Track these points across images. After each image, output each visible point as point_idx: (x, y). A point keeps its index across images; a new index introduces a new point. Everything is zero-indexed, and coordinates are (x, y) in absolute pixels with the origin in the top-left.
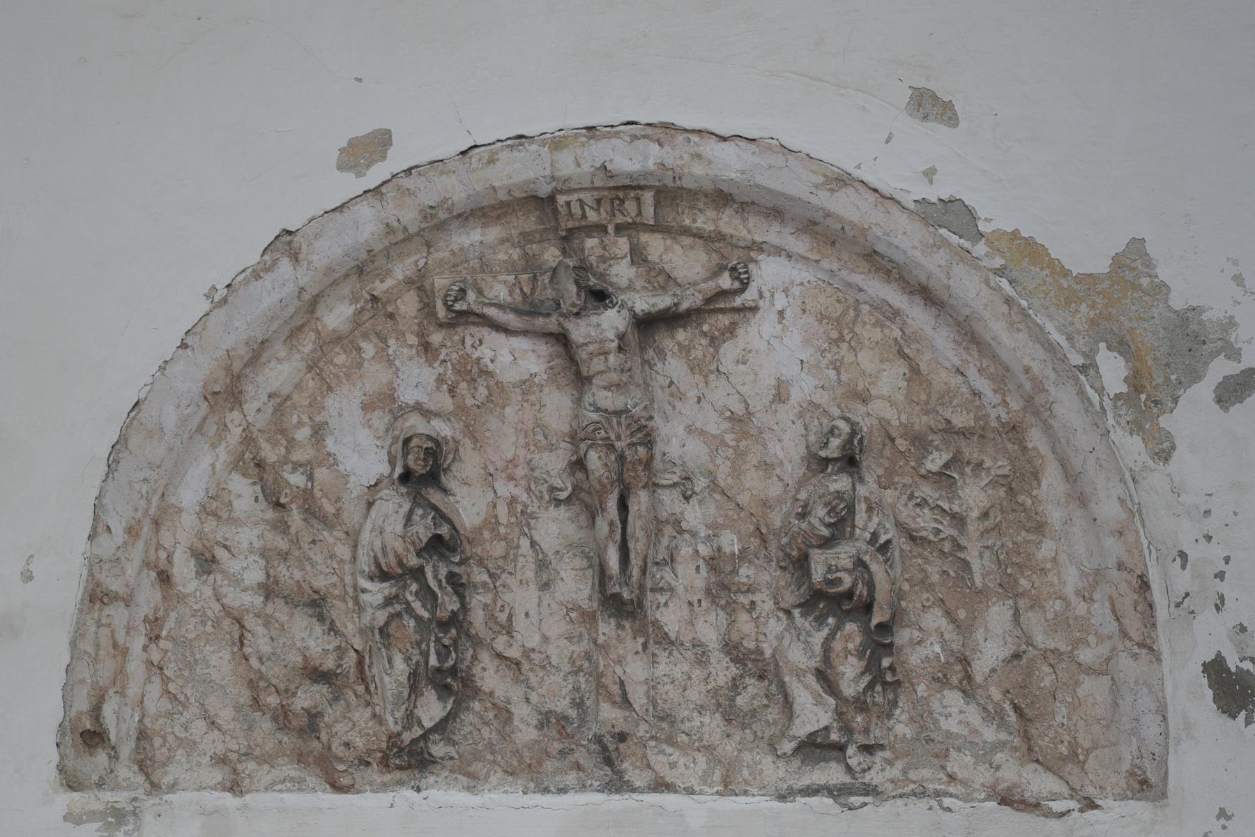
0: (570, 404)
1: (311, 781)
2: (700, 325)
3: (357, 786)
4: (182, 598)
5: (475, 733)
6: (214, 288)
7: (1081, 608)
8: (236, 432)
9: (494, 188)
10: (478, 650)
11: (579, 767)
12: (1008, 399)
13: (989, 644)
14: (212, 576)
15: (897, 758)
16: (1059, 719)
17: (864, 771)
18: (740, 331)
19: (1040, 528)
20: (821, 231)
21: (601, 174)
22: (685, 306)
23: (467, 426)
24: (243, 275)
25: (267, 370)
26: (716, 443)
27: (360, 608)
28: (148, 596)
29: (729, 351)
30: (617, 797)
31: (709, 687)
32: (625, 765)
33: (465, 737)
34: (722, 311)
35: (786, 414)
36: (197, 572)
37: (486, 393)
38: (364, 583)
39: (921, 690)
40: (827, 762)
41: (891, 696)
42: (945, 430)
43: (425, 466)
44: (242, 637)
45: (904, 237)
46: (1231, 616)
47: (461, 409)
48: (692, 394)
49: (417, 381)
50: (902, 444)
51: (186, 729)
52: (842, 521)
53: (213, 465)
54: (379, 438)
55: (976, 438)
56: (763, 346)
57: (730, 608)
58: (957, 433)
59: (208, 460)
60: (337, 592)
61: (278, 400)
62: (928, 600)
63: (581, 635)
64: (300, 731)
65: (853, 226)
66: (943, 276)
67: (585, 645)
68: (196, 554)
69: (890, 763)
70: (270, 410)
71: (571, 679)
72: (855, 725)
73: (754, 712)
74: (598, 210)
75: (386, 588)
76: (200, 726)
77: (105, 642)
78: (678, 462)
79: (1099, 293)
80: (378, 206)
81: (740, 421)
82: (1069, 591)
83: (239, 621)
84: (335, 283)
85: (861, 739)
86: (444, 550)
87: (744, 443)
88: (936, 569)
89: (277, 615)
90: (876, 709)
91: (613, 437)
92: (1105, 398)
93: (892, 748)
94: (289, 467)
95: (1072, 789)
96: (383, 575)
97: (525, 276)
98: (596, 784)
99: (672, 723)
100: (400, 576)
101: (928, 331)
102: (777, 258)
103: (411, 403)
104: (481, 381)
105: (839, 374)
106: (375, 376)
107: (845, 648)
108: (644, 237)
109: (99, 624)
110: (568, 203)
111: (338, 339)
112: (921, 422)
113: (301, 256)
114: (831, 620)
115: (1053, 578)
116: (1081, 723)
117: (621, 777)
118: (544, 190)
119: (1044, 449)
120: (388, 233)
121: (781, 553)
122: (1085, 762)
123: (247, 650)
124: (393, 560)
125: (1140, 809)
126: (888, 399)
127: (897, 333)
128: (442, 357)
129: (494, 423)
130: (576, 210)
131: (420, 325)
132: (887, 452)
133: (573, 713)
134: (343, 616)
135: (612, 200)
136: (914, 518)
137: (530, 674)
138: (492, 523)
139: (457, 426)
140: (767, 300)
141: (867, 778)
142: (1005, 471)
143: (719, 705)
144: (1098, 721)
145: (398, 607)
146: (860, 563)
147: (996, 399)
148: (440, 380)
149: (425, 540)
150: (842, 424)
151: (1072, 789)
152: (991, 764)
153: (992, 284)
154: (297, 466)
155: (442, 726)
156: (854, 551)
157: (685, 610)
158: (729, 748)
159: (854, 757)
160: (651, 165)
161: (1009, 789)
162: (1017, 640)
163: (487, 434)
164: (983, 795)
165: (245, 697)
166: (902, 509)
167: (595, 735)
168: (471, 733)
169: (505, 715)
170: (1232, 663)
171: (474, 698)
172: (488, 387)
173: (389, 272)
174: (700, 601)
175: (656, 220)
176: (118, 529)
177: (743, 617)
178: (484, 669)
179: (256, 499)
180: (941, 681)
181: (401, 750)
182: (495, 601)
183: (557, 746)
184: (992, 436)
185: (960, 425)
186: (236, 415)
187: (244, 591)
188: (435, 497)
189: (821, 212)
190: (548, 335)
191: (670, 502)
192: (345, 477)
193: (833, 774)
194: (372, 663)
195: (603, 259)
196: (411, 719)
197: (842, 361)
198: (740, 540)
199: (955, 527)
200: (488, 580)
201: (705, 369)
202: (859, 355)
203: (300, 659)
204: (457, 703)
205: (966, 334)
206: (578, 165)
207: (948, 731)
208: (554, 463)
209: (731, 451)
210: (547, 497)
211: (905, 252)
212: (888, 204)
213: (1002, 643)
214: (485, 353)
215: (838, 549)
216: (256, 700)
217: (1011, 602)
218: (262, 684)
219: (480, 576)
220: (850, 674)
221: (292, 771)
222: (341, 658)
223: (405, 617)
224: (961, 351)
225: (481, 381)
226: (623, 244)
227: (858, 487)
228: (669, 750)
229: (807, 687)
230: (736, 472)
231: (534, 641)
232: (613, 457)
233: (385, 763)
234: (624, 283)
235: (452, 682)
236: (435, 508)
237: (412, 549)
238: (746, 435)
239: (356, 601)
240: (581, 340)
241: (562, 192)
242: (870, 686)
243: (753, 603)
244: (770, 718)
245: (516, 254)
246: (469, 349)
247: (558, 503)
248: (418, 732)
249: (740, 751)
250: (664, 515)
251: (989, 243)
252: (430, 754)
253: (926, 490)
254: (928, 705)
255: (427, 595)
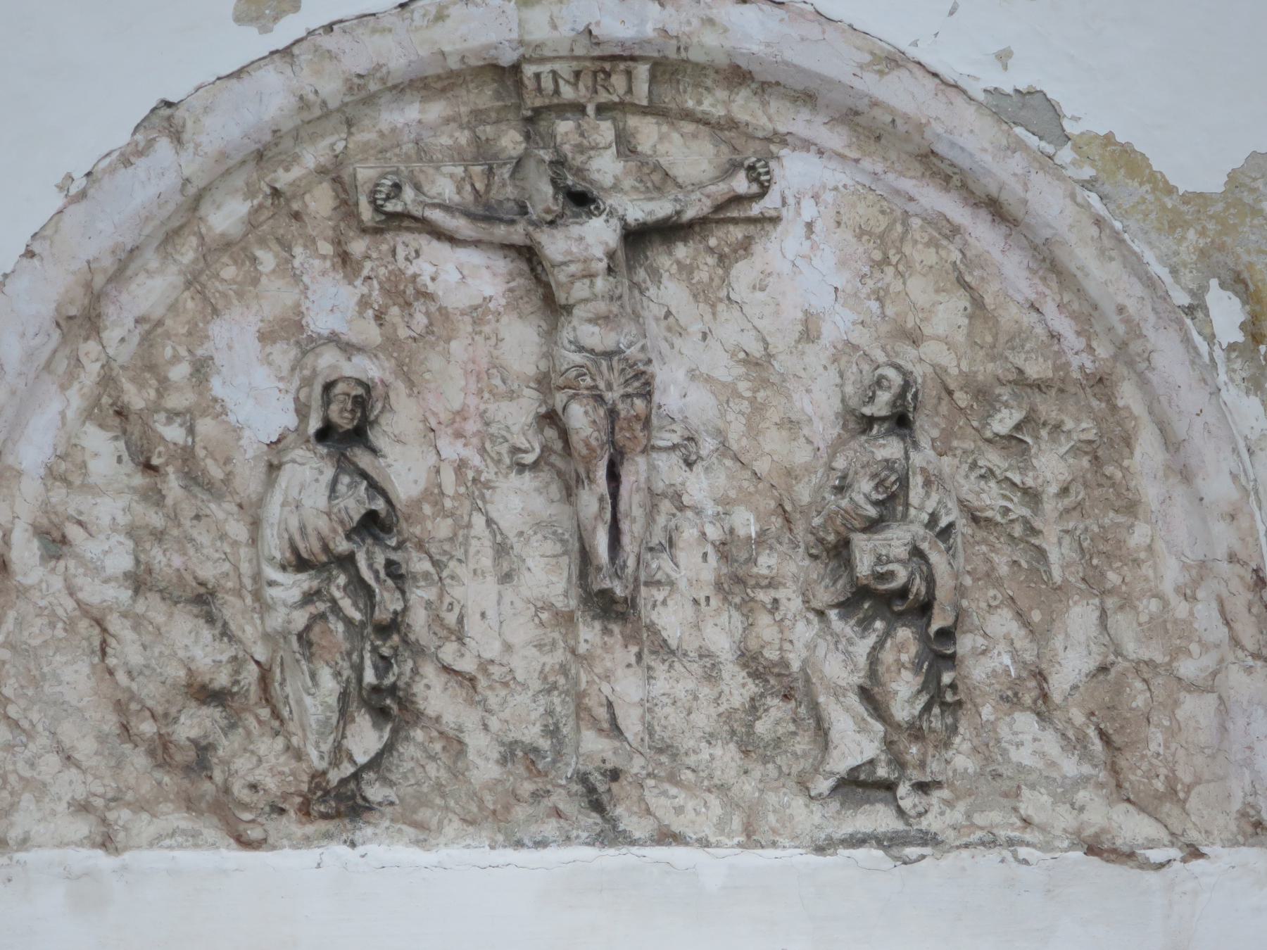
0: (536, 338)
2: (705, 238)
3: (271, 841)
5: (419, 770)
6: (70, 178)
7: (1181, 609)
8: (93, 369)
9: (443, 53)
10: (420, 661)
11: (558, 814)
12: (1094, 344)
13: (1070, 654)
14: (62, 563)
15: (958, 798)
16: (1153, 747)
17: (920, 815)
18: (757, 248)
19: (1131, 507)
20: (865, 125)
21: (585, 41)
22: (690, 214)
23: (400, 365)
24: (108, 160)
25: (133, 287)
27: (263, 606)
29: (743, 272)
30: (612, 851)
31: (721, 709)
32: (619, 811)
33: (405, 777)
34: (735, 221)
35: (816, 356)
36: (42, 557)
37: (425, 321)
38: (272, 573)
39: (987, 712)
40: (872, 803)
41: (949, 721)
42: (1015, 383)
43: (352, 420)
44: (104, 643)
45: (972, 138)
48: (696, 328)
49: (332, 304)
50: (962, 398)
51: (32, 765)
52: (892, 497)
53: (63, 414)
54: (281, 379)
55: (1053, 392)
56: (786, 268)
57: (747, 608)
58: (1030, 386)
59: (55, 406)
60: (230, 585)
61: (147, 327)
62: (995, 598)
63: (554, 643)
64: (187, 769)
65: (907, 118)
66: (1019, 188)
67: (560, 656)
68: (41, 533)
69: (949, 804)
70: (136, 339)
71: (542, 700)
72: (908, 757)
73: (778, 741)
74: (575, 85)
75: (300, 583)
76: (53, 760)
78: (677, 416)
79: (1211, 217)
80: (288, 71)
81: (757, 365)
82: (1167, 587)
83: (99, 622)
84: (228, 172)
85: (917, 776)
86: (377, 531)
87: (761, 395)
88: (1005, 559)
89: (151, 614)
90: (932, 736)
91: (602, 385)
92: (1216, 348)
93: (951, 785)
94: (162, 417)
95: (1173, 834)
96: (301, 564)
97: (478, 169)
98: (584, 835)
99: (674, 757)
100: (324, 565)
101: (996, 254)
102: (804, 154)
103: (325, 333)
104: (419, 306)
105: (882, 306)
106: (276, 297)
107: (898, 661)
108: (633, 121)
110: (538, 76)
111: (226, 245)
112: (986, 370)
113: (186, 136)
114: (879, 624)
115: (1146, 570)
116: (1181, 752)
117: (615, 827)
118: (507, 57)
119: (1138, 408)
120: (301, 108)
121: (811, 538)
122: (1185, 801)
123: (111, 661)
124: (316, 546)
127: (956, 256)
128: (365, 272)
129: (435, 362)
130: (547, 83)
131: (335, 228)
132: (944, 409)
133: (545, 744)
134: (239, 617)
135: (595, 74)
136: (978, 494)
137: (489, 693)
138: (434, 494)
139: (386, 364)
140: (792, 208)
141: (924, 824)
142: (1091, 435)
143: (733, 732)
144: (1202, 750)
145: (321, 606)
146: (917, 552)
147: (1080, 343)
148: (364, 303)
149: (357, 518)
150: (891, 373)
151: (1173, 834)
152: (1072, 805)
153: (1079, 199)
154: (173, 415)
155: (375, 763)
156: (908, 537)
157: (690, 609)
158: (748, 788)
160: (649, 31)
161: (1097, 835)
162: (1103, 649)
163: (427, 376)
164: (1066, 843)
165: (111, 723)
166: (962, 481)
167: (577, 772)
168: (412, 770)
169: (456, 746)
171: (416, 724)
172: (428, 314)
173: (296, 158)
174: (708, 599)
175: (650, 100)
177: (764, 619)
178: (428, 687)
179: (120, 460)
180: (1011, 701)
181: (327, 792)
182: (441, 597)
183: (527, 787)
184: (1073, 390)
185: (1035, 376)
186: (92, 347)
187: (106, 581)
188: (363, 459)
189: (866, 100)
190: (508, 248)
191: (669, 469)
192: (237, 430)
194: (284, 680)
195: (580, 149)
196: (339, 753)
197: (887, 291)
198: (758, 519)
199: (1027, 505)
200: (432, 570)
202: (908, 283)
203: (182, 673)
204: (395, 732)
205: (1044, 260)
206: (555, 27)
207: (1019, 764)
208: (517, 417)
209: (746, 403)
210: (507, 461)
211: (971, 155)
212: (952, 93)
213: (1085, 653)
214: (423, 268)
215: (888, 534)
216: (125, 728)
217: (1097, 601)
218: (134, 706)
220: (904, 693)
222: (237, 672)
223: (332, 618)
224: (1037, 281)
225: (419, 306)
227: (912, 454)
228: (673, 791)
229: (847, 710)
230: (753, 431)
231: (492, 650)
232: (602, 412)
233: (305, 811)
234: (608, 181)
235: (389, 705)
236: (364, 475)
237: (340, 530)
238: (765, 383)
239: (257, 596)
240: (559, 258)
241: (530, 61)
242: (927, 708)
243: (776, 601)
244: (799, 749)
245: (463, 137)
246: (401, 263)
247: (521, 468)
248: (347, 770)
249: (762, 791)
250: (659, 486)
251: (1077, 148)
252: (365, 799)
253: (993, 458)
254: (995, 731)
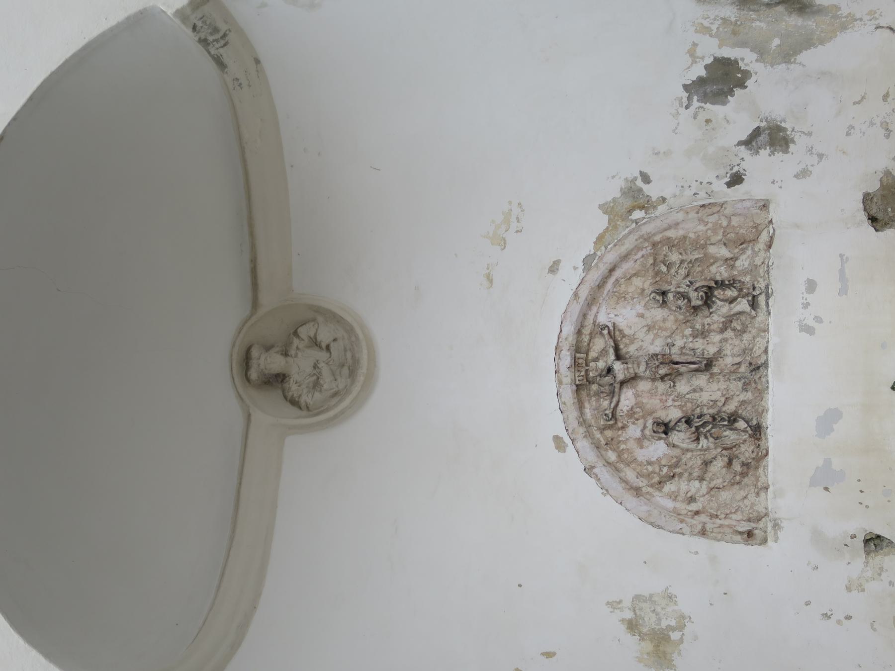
1: (764, 463)
4: (704, 507)
7: (710, 225)
8: (649, 489)
19: (685, 237)
20: (592, 301)
26: (657, 336)
27: (708, 449)
28: (703, 518)
29: (627, 332)
35: (647, 314)
39: (736, 273)
45: (595, 276)
46: (714, 180)
47: (643, 417)
48: (640, 343)
49: (634, 431)
52: (682, 296)
57: (709, 331)
59: (658, 498)
64: (748, 468)
67: (721, 377)
68: (689, 503)
73: (743, 324)
75: (702, 438)
77: (718, 530)
81: (650, 328)
82: (705, 228)
96: (698, 439)
106: (632, 444)
108: (590, 358)
109: (712, 532)
111: (619, 456)
112: (651, 273)
115: (700, 234)
118: (575, 388)
119: (661, 236)
125: (772, 207)
126: (644, 283)
129: (648, 406)
130: (581, 378)
133: (743, 381)
138: (681, 407)
146: (696, 290)
148: (634, 423)
155: (747, 422)
159: (757, 292)
160: (568, 353)
165: (737, 487)
170: (727, 179)
173: (598, 439)
176: (681, 526)
177: (712, 327)
180: (733, 267)
183: (753, 385)
188: (672, 424)
190: (620, 389)
191: (675, 350)
192: (665, 455)
193: (762, 299)
195: (597, 370)
196: (745, 431)
201: (633, 340)
208: (662, 387)
214: (625, 409)
219: (698, 411)
220: (730, 293)
221: (761, 470)
226: (592, 364)
230: (666, 330)
231: (719, 393)
233: (759, 439)
235: (733, 419)
238: (654, 326)
239: (705, 450)
245: (593, 399)
247: (674, 386)
253: (673, 271)
255: (704, 425)
